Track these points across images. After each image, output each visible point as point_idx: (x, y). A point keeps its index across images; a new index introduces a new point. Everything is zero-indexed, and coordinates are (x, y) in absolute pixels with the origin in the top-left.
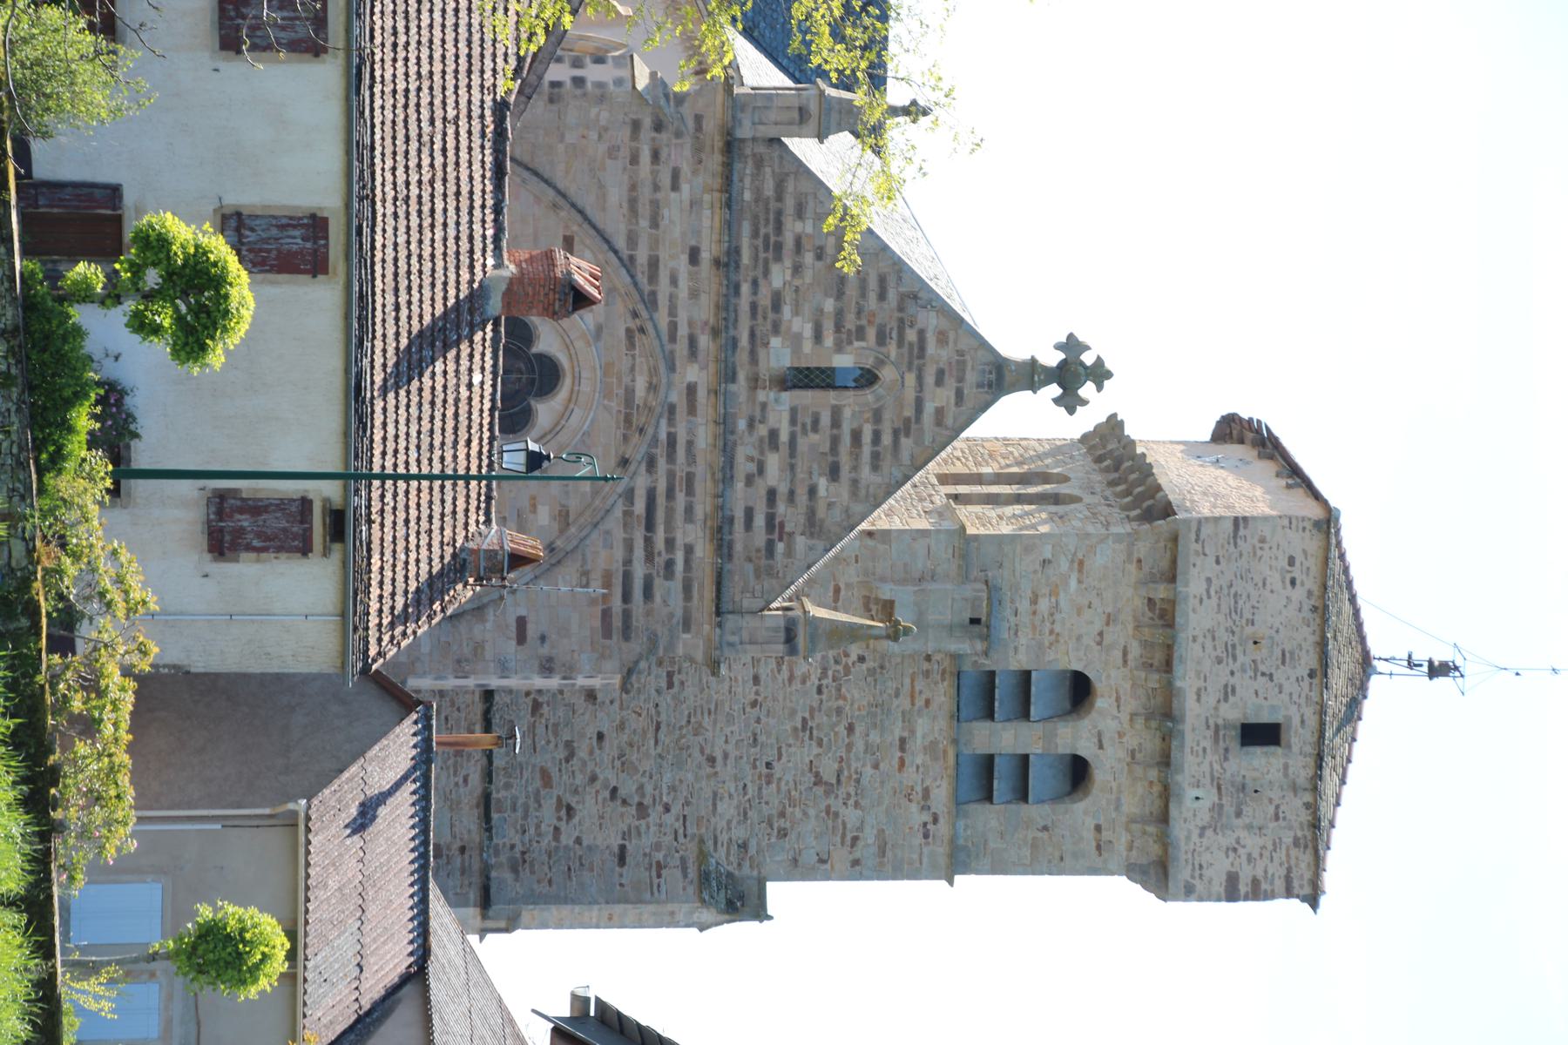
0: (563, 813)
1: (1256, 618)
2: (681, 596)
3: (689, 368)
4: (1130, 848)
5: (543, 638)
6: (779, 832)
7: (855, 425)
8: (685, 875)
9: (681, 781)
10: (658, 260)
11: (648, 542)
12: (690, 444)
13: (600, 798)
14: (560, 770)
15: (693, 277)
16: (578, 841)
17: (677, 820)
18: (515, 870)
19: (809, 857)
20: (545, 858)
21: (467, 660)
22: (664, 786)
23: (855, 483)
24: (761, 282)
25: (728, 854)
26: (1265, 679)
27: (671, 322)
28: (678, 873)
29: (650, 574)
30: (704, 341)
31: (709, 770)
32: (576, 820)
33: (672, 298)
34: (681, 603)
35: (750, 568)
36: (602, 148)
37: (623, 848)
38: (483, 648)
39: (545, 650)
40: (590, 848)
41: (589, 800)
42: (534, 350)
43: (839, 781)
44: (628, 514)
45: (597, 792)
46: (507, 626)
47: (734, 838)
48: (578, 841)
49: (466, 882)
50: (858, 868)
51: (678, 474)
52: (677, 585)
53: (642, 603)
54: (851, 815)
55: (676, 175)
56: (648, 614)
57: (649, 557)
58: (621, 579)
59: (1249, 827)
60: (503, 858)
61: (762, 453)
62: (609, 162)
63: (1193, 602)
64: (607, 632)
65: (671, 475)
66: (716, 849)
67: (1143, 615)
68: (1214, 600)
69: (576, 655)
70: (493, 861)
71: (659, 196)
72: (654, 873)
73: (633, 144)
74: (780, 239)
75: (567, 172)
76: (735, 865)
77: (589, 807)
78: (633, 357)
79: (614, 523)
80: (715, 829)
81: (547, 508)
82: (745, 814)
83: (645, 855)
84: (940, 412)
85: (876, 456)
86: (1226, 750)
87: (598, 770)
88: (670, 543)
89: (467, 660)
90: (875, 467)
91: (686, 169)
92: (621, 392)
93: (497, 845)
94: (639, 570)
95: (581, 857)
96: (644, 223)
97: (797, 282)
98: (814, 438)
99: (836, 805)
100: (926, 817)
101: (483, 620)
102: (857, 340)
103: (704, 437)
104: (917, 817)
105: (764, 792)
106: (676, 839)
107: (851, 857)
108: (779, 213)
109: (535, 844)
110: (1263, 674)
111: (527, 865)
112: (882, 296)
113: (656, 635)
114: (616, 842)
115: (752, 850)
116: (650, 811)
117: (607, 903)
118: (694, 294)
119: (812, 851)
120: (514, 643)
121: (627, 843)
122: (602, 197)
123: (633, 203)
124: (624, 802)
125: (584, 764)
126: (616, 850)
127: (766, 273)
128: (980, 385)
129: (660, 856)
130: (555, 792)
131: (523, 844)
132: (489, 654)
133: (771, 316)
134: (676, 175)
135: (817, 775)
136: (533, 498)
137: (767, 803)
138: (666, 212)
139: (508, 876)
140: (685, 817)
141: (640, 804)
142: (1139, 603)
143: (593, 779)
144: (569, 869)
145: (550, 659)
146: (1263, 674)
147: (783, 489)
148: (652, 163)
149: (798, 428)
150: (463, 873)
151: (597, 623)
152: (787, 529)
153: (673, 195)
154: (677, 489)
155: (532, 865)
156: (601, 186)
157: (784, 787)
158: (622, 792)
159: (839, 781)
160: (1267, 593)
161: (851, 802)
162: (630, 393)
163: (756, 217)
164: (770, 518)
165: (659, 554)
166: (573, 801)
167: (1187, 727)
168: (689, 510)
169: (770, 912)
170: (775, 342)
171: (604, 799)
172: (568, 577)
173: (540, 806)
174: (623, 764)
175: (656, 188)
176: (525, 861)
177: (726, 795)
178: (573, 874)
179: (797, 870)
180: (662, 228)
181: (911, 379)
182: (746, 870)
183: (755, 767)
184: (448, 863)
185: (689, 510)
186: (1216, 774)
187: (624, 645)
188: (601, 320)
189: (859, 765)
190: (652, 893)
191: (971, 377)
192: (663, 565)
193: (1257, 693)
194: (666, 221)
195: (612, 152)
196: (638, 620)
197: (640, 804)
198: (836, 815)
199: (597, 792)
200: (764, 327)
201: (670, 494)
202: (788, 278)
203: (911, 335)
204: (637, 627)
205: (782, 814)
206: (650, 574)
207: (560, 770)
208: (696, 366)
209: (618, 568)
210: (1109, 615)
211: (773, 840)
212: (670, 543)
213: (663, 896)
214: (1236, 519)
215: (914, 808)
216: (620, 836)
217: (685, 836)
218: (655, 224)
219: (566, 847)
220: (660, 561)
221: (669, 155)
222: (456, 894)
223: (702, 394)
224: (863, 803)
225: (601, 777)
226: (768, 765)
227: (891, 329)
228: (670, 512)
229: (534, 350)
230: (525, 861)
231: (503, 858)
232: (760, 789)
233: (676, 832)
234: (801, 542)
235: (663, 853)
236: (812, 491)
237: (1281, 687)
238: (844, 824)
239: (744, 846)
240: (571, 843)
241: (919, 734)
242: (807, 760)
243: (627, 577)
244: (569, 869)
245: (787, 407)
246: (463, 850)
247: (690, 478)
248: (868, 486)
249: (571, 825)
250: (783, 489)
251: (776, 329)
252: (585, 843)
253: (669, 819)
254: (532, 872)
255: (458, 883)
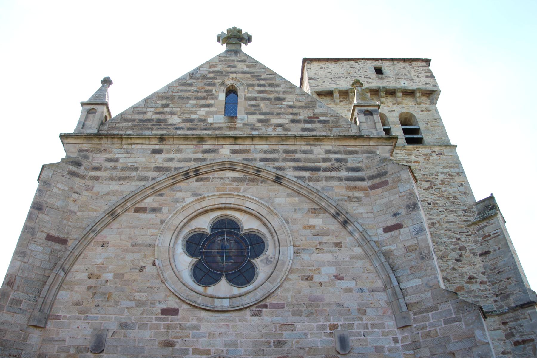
0: (474, 280)
1: (341, 73)
2: (355, 155)
3: (222, 153)
4: (426, 104)
5: (395, 215)
6: (455, 199)
7: (256, 92)
8: (486, 226)
9: (445, 235)
10: (157, 167)
11: (325, 170)
12: (266, 152)
13: (462, 266)
14: (454, 283)
15: (168, 152)
16: (483, 273)
17: (462, 235)
18: (508, 296)
19: (462, 189)
20: (497, 285)
21: (420, 254)
22: (449, 241)
23: (284, 92)
24: (177, 126)
25: (470, 216)
26: (361, 71)
27: (194, 161)
28: (486, 229)
29: (345, 168)
30: (206, 147)
31: (438, 225)
32: (475, 275)
33: (180, 161)
34: (360, 155)
35: (334, 129)
36: (85, 193)
37: (481, 255)
38: (410, 246)
39: (403, 212)
40: (485, 268)
41: (464, 270)
42: (209, 231)
43: (429, 181)
44: (310, 179)
45: (459, 267)
46: (392, 236)
47: (463, 214)
48: (483, 273)
49: (522, 316)
50: (460, 174)
51: (284, 157)
52: (350, 157)
53: (363, 172)
54: (441, 177)
55: (109, 160)
56: (369, 168)
57: (336, 169)
58: (351, 182)
59: (410, 73)
60: (503, 304)
61: (271, 125)
62: (94, 190)
63: (338, 86)
64: (386, 183)
65: (285, 160)
66: (470, 221)
67: (346, 103)
68: (336, 82)
69: (401, 195)
70: (506, 308)
71: (119, 167)
72: (489, 238)
73: (87, 178)
74: (155, 120)
75: (96, 210)
76: (474, 213)
77: (468, 270)
78: (213, 178)
79: (319, 186)
80: (462, 221)
81: (310, 220)
82: (451, 211)
83: (481, 245)
84: (248, 66)
85: (271, 86)
86: (386, 77)
87: (450, 268)
88: (325, 160)
89: (420, 254)
90: (277, 86)
91: (108, 156)
92: (235, 184)
93: (497, 308)
94: (344, 174)
95: (491, 270)
96: (134, 174)
97: (179, 113)
98: (262, 106)
99: (438, 182)
100: (434, 154)
101: (391, 251)
102: (212, 92)
103: (263, 146)
104: (435, 157)
105: (440, 205)
106: (470, 235)
107: (457, 176)
108: (141, 120)
109: (491, 292)
110: (359, 71)
111: (502, 292)
112: (191, 85)
113: (380, 160)
114: (479, 259)
115: (466, 208)
116: (462, 245)
117: (510, 251)
118: (179, 151)
119: (459, 188)
120: (402, 230)
121: (478, 254)
122: (114, 193)
123: (120, 179)
124: (461, 256)
125: (448, 273)
126: (483, 257)
127: (172, 125)
128: (237, 56)
129: (480, 239)
130: (465, 285)
131: (492, 297)
132: (414, 242)
133: (195, 123)
134: (109, 160)
135: (429, 188)
136: (305, 227)
137: (445, 204)
138: (129, 164)
139: (512, 298)
140: (460, 233)
141: (460, 249)
142: (341, 104)
143: (454, 269)
144: (499, 273)
145: (408, 206)
146: (359, 71)
147: (291, 117)
148: (100, 170)
149: (257, 112)
150: (518, 320)
151: (380, 190)
152: (312, 115)
153: (121, 161)
154: (293, 157)
155: (503, 289)
156: (108, 194)
157: (437, 199)
158: (457, 257)
159: (429, 181)
160: (332, 72)
161: (436, 177)
162: (235, 179)
163: (141, 129)
164: (306, 122)
165: (332, 165)
166: (466, 278)
167: (381, 86)
168: (305, 152)
169: (490, 195)
170: (210, 121)
171: (462, 264)
172: (354, 208)
173: (473, 291)
174: (444, 257)
175: (115, 168)
176: (501, 293)
177: (446, 218)
178: (501, 270)
179: (468, 192)
180: (137, 166)
181: (232, 75)
182: (474, 209)
183: (432, 209)
184: (515, 328)
185: (305, 152)
186: (395, 79)
187: (390, 173)
188: (189, 194)
189: (420, 175)
190: (499, 235)
191: (233, 58)
192: (338, 164)
193: (366, 71)
194: (135, 164)
195: (89, 189)
196: (374, 171)
197: (460, 249)
198: (442, 181)
199: (459, 267)
200: (202, 125)
201: (295, 160)
202: (176, 116)
203: (212, 75)
204: (378, 171)
205: (448, 198)
206: (345, 168)
207: (454, 283)
208: (220, 150)
209: (344, 183)
210: (347, 111)
211: (459, 201)
212: (325, 160)
213: (499, 231)
214: (309, 79)
215: (431, 158)
216: (476, 257)
217: (468, 232)
218: (136, 169)
219: (488, 278)
220: (336, 165)
221: (97, 163)
222: (531, 319)
223: (236, 147)
224: (435, 173)
225: (452, 266)
226: (429, 204)
227: (207, 81)
228: (306, 160)
229: (209, 231)
230: (501, 293)
231: (503, 304)
232: (440, 206)
233: (467, 235)
234: (317, 111)
235: (478, 238)
236: (291, 107)
237: (362, 67)
238: (445, 179)
239: (465, 211)
240: (485, 277)
241: (404, 158)
242: (424, 191)
243: (348, 179)
244: (499, 273)
245: (246, 116)
246: (504, 323)
247: (285, 152)
248: (286, 88)
249: (477, 277)
250: (291, 117)
251: (204, 120)
252: (484, 271)
253: (463, 238)
254: (506, 288)
255: (524, 320)
